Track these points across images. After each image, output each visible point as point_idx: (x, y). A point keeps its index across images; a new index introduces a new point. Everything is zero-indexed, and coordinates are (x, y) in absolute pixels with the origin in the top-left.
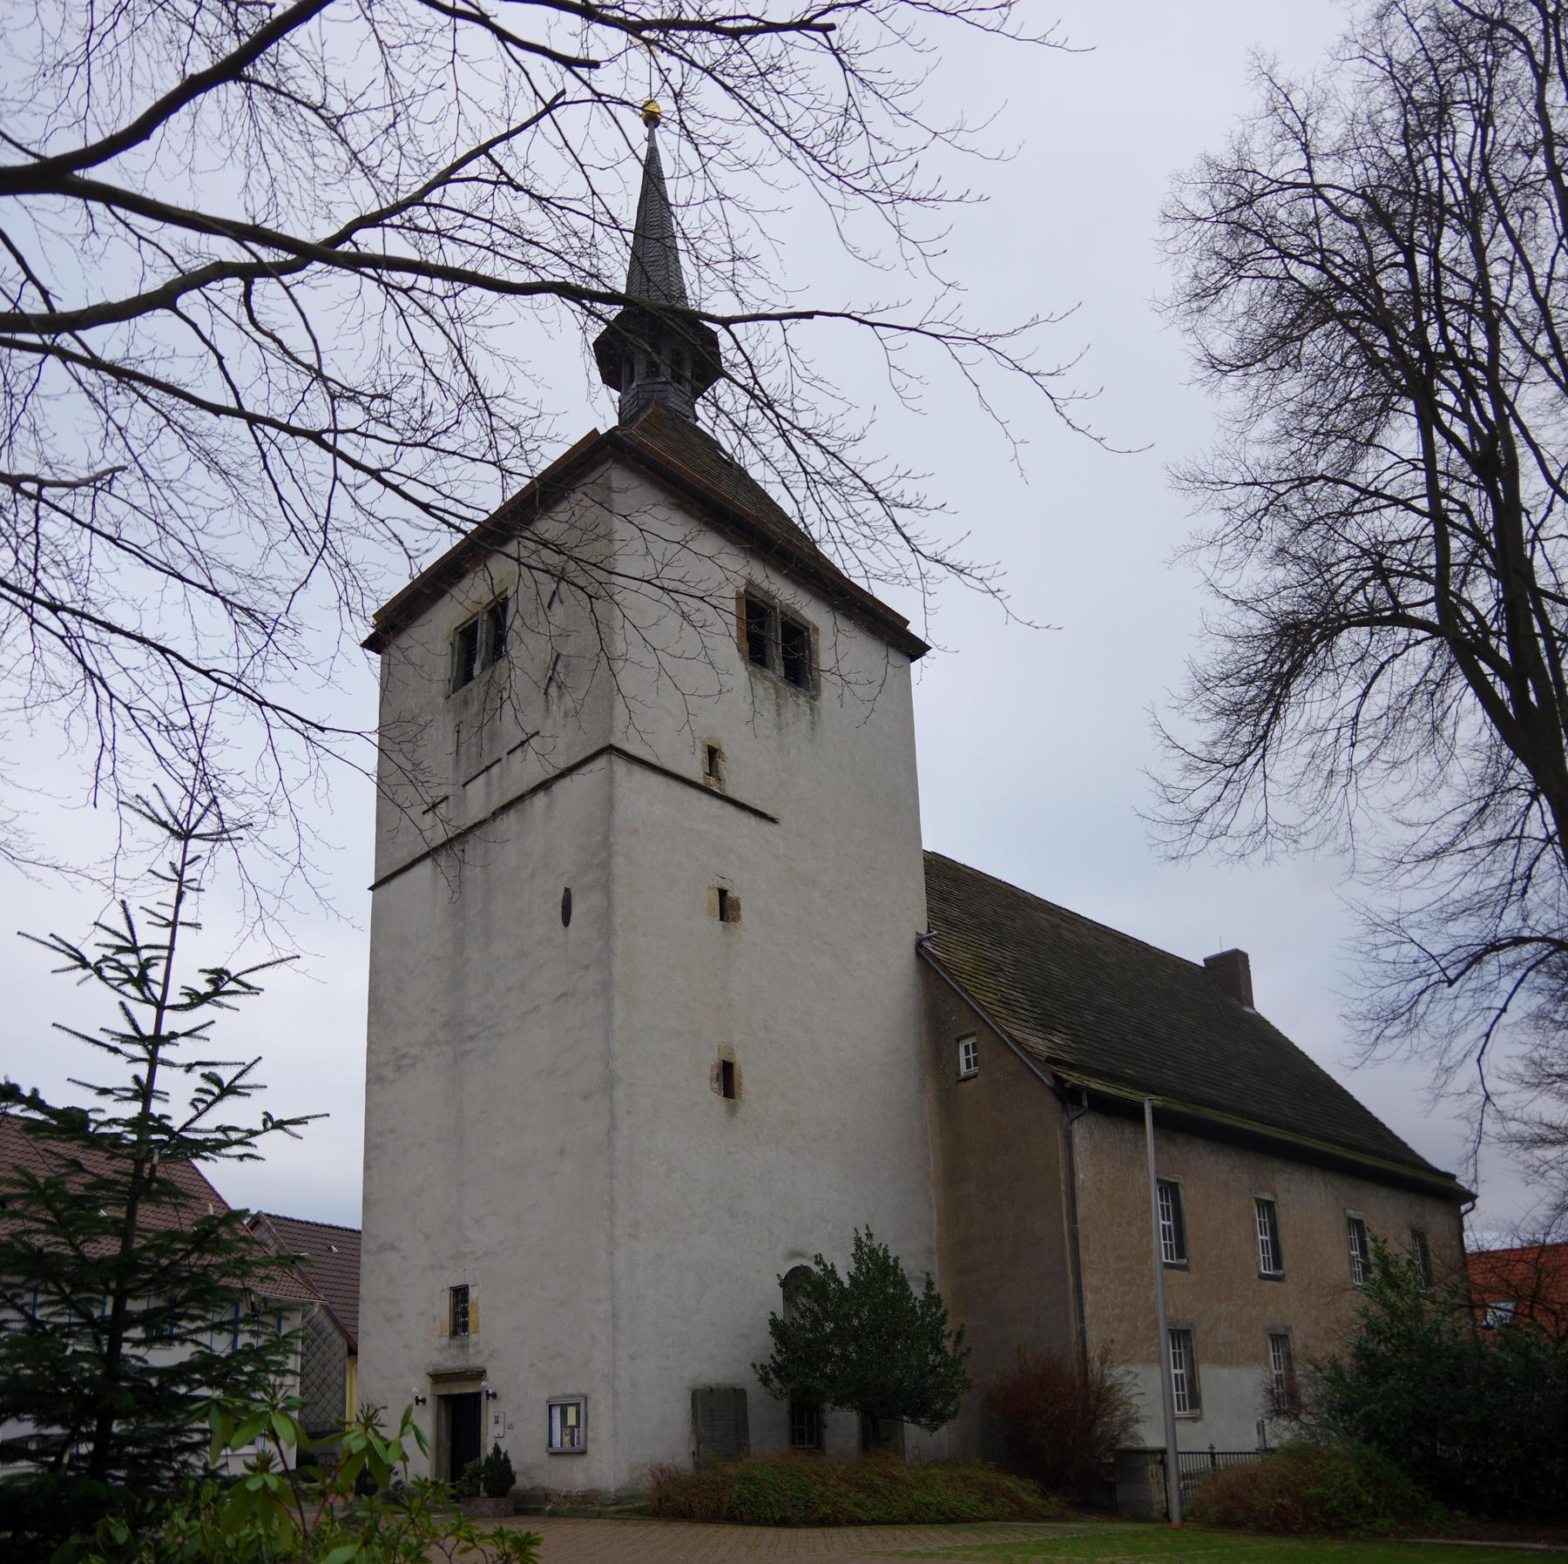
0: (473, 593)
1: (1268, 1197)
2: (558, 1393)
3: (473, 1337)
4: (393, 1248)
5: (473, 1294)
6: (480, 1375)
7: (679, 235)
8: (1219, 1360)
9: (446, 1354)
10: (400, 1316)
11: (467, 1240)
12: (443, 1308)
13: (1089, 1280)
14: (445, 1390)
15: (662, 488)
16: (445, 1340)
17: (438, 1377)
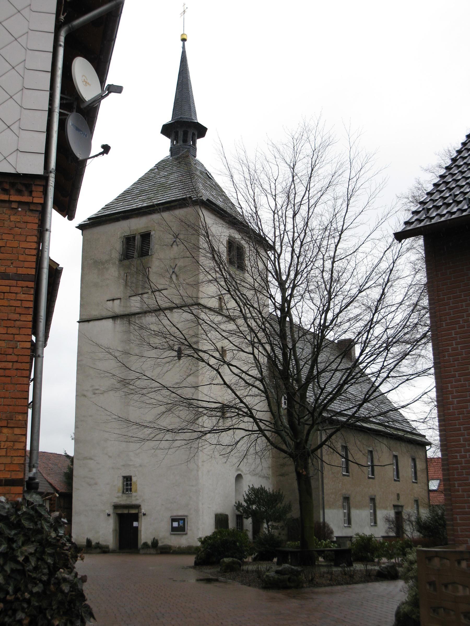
0: (137, 225)
1: (370, 449)
2: (175, 514)
3: (134, 494)
4: (91, 459)
5: (134, 479)
6: (138, 507)
7: (414, 523)
8: (357, 507)
9: (120, 499)
10: (96, 484)
11: (131, 460)
12: (119, 483)
13: (325, 481)
14: (120, 511)
15: (215, 215)
16: (120, 494)
17: (116, 507)
